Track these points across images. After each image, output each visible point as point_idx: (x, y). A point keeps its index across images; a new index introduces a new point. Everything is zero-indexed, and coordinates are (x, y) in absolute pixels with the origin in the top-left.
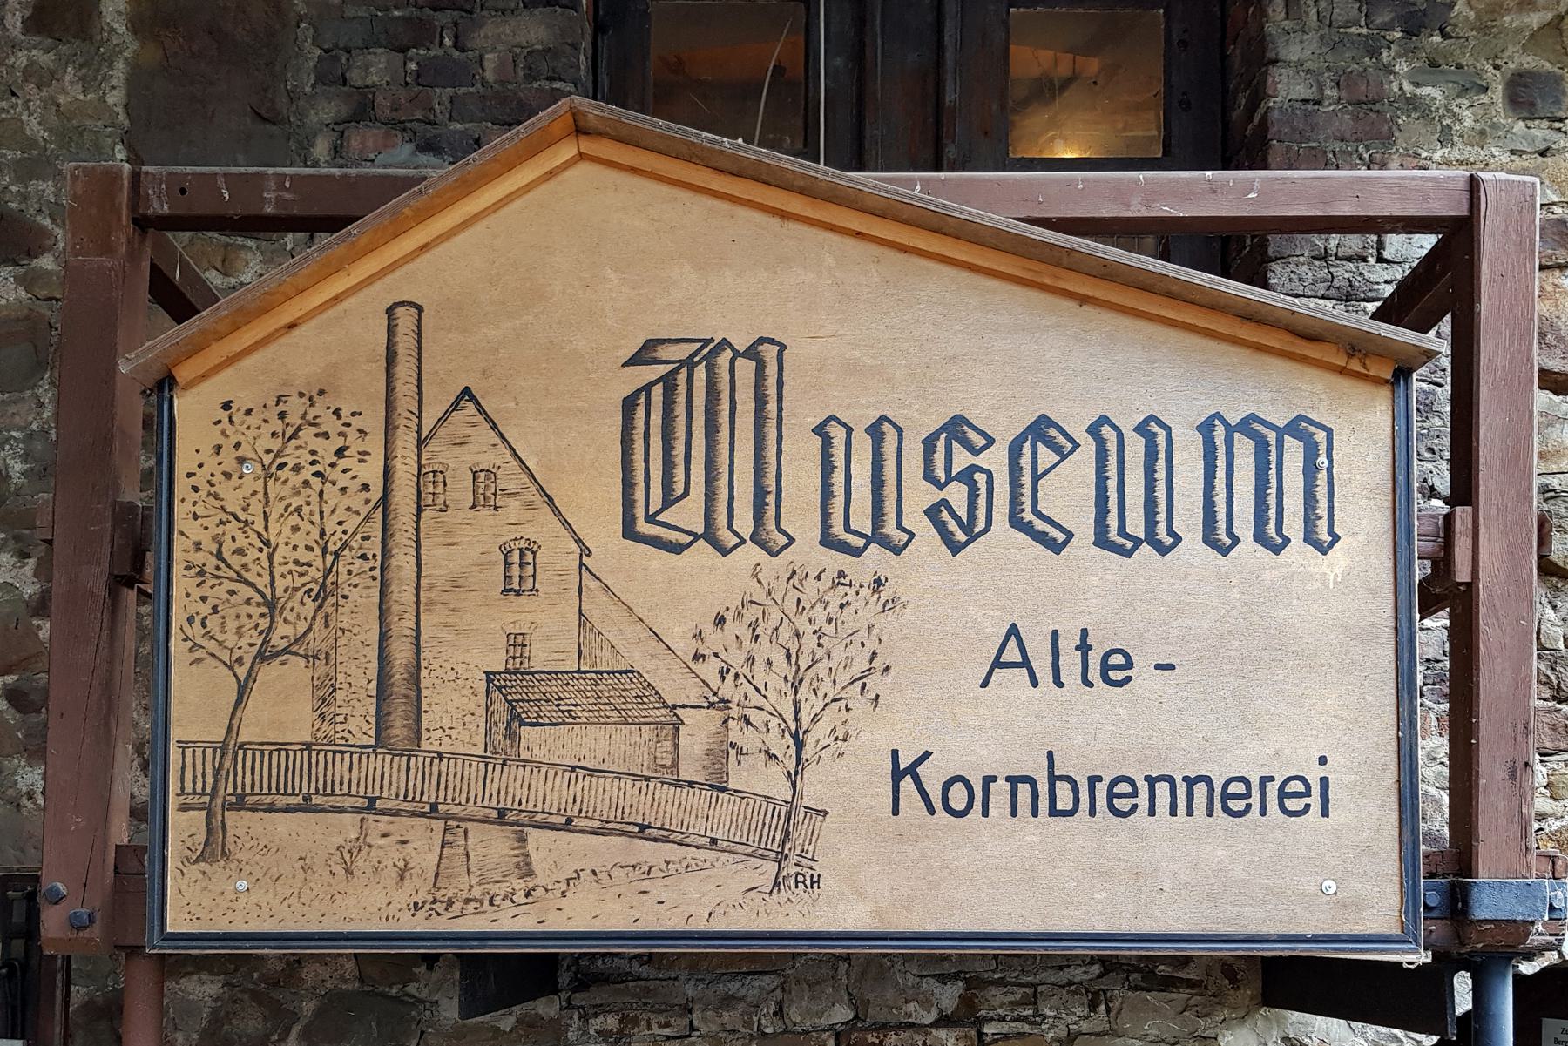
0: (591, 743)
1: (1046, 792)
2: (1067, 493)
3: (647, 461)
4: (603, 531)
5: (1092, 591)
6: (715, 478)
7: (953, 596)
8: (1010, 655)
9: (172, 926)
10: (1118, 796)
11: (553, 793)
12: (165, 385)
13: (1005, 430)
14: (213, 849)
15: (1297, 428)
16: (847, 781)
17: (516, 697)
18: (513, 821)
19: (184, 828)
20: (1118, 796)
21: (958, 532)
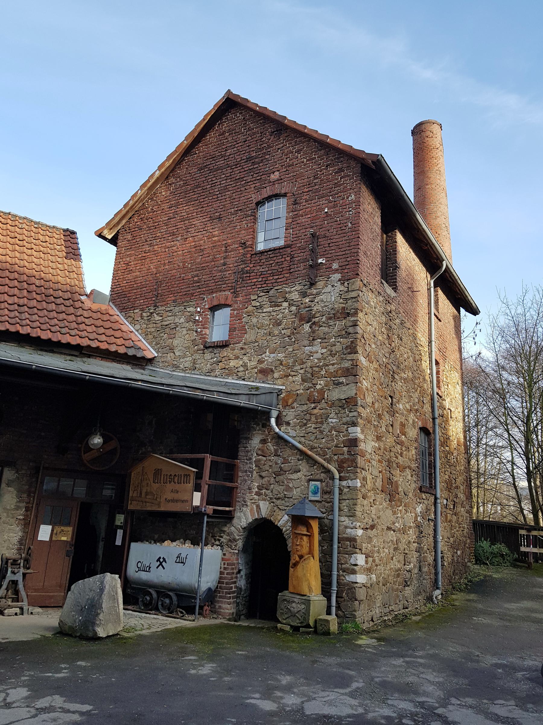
0: (150, 497)
1: (173, 501)
2: (176, 480)
3: (163, 384)
4: (152, 482)
5: (177, 486)
6: (201, 391)
7: (170, 486)
8: (172, 491)
9: (119, 518)
10: (177, 501)
11: (147, 500)
12: (131, 473)
13: (173, 475)
14: (131, 504)
15: (189, 475)
16: (163, 500)
17: (147, 494)
18: (146, 502)
19: (130, 502)
20: (177, 501)
21: (170, 482)
